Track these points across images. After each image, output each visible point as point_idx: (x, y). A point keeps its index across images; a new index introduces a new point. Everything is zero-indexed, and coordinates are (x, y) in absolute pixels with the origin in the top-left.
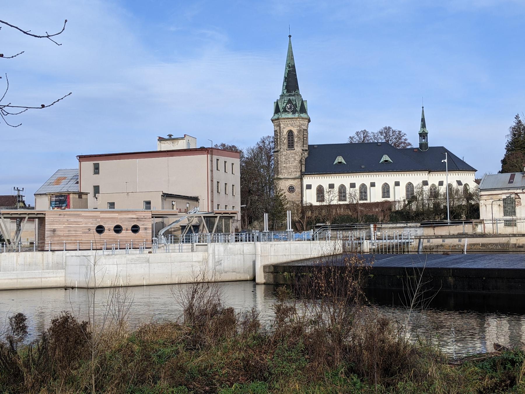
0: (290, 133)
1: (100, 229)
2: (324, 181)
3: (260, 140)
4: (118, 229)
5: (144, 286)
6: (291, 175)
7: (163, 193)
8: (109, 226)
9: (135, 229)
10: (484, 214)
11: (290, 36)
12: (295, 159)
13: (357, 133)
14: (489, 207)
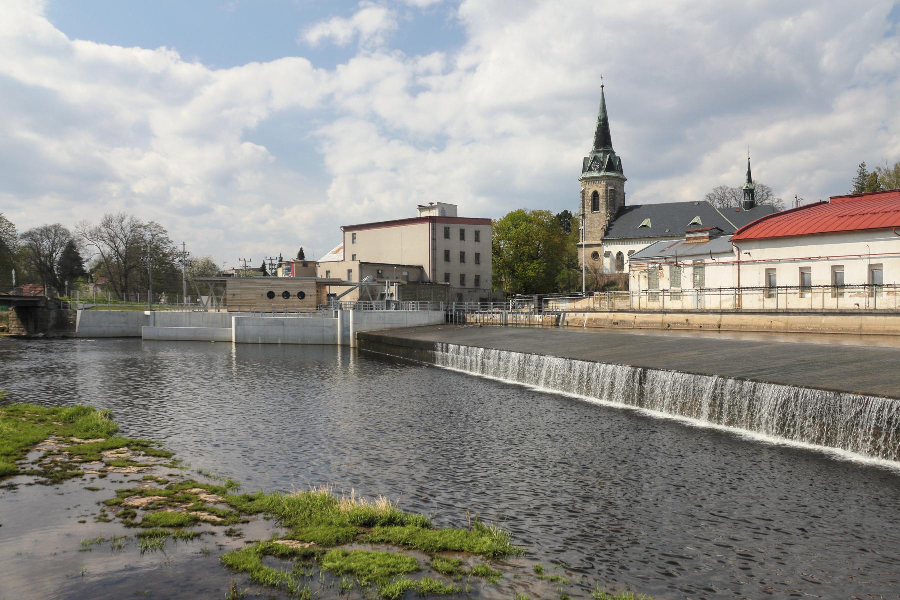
0: (596, 194)
1: (271, 295)
3: (137, 219)
4: (287, 295)
5: (308, 345)
6: (595, 241)
7: (360, 263)
8: (279, 292)
9: (302, 295)
10: (633, 286)
11: (603, 87)
12: (600, 223)
14: (637, 278)
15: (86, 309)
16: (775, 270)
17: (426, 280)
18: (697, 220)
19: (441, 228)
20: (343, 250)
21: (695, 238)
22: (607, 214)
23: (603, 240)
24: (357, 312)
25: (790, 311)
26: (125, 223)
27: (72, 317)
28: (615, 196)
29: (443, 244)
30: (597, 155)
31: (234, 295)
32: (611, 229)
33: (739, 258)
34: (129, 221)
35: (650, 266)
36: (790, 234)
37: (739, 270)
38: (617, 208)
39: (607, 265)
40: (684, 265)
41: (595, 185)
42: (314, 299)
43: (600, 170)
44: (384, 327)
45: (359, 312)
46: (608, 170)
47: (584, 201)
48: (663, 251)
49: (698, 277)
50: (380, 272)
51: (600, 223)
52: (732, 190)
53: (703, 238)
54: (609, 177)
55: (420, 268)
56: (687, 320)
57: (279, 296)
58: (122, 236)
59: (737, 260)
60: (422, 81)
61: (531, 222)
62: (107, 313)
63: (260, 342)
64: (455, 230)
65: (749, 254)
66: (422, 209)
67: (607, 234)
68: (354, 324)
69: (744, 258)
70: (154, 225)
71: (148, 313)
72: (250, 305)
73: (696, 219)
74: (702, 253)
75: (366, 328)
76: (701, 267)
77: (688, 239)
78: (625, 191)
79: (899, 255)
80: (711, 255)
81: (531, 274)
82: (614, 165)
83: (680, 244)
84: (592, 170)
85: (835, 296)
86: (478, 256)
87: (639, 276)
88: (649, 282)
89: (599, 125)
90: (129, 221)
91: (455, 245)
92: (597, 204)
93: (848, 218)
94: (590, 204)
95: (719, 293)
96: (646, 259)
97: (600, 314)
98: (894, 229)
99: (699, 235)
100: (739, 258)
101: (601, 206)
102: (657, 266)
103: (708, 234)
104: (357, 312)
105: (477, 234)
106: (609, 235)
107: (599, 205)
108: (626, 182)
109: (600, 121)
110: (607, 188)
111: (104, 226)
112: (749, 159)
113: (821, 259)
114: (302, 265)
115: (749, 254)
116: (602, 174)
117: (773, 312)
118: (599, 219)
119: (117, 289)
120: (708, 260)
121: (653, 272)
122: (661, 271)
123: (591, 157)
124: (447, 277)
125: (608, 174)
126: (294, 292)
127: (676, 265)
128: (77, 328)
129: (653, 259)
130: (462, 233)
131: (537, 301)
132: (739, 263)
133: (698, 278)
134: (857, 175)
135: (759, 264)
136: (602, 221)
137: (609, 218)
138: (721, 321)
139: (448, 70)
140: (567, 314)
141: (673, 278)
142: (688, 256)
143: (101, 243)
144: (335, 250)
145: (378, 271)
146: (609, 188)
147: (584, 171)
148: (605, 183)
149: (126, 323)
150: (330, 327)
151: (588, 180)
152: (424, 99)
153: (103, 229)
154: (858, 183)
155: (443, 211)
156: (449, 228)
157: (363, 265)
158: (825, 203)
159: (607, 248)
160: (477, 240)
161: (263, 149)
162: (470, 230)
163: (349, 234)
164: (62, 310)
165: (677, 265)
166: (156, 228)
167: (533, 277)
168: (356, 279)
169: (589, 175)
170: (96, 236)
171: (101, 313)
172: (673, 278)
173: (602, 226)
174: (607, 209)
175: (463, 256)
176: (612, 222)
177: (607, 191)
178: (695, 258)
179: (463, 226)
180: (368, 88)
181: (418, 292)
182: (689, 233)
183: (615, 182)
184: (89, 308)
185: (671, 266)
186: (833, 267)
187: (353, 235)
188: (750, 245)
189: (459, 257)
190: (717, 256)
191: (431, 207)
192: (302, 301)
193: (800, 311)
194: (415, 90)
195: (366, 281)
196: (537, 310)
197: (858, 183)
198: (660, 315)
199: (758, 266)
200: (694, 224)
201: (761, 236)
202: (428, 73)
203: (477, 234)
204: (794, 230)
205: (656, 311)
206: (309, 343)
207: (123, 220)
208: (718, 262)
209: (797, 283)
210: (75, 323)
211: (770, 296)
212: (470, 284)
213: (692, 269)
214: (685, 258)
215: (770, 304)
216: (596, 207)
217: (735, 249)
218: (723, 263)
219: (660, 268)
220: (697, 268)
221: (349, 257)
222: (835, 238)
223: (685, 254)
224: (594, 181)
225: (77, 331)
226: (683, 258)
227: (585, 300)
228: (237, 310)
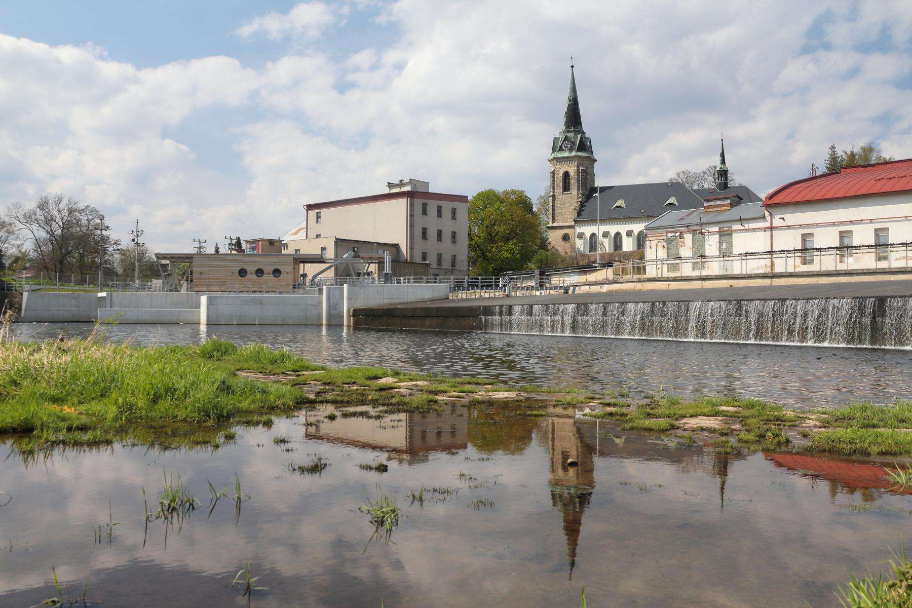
0: (566, 174)
2: (598, 229)
4: (260, 272)
6: (566, 222)
7: (336, 239)
8: (251, 269)
9: (277, 272)
11: (572, 67)
12: (571, 204)
13: (678, 175)
14: (654, 248)
15: (32, 291)
17: (402, 259)
18: (672, 200)
19: (418, 203)
20: (305, 230)
21: (715, 206)
22: (578, 195)
23: (575, 221)
24: (352, 286)
25: (853, 272)
26: (62, 205)
27: (17, 299)
29: (420, 222)
30: (568, 135)
31: (201, 273)
32: (584, 210)
33: (771, 224)
34: (67, 202)
35: (669, 235)
36: (842, 195)
37: (772, 236)
38: (588, 188)
39: (580, 244)
40: (709, 232)
41: (565, 165)
42: (291, 276)
43: (571, 150)
44: (382, 302)
45: (355, 286)
46: (579, 149)
47: (553, 181)
48: (682, 219)
49: (724, 245)
50: (356, 249)
51: (571, 204)
52: (695, 174)
53: (724, 205)
54: (580, 157)
55: (396, 247)
56: (731, 286)
57: (251, 273)
58: (58, 220)
59: (770, 225)
60: (350, 77)
61: (502, 202)
62: (56, 295)
63: (235, 323)
64: (432, 206)
65: (783, 219)
66: (392, 186)
67: (579, 215)
68: (349, 299)
69: (777, 222)
70: (90, 208)
71: (104, 294)
72: (220, 283)
73: (671, 199)
74: (730, 219)
75: (362, 304)
76: (728, 235)
77: (706, 207)
80: (741, 221)
81: (506, 255)
82: (584, 146)
83: (695, 214)
84: (563, 150)
86: (454, 235)
87: (657, 246)
88: (668, 252)
89: (569, 105)
90: (67, 202)
91: (432, 223)
92: (567, 185)
93: (886, 181)
94: (561, 184)
96: (665, 227)
97: (623, 284)
99: (718, 203)
100: (771, 224)
101: (572, 187)
102: (678, 234)
103: (729, 202)
104: (352, 286)
105: (454, 211)
106: (582, 215)
107: (569, 186)
109: (570, 101)
110: (578, 168)
111: (39, 208)
112: (722, 140)
113: (863, 222)
114: (268, 243)
115: (783, 219)
116: (574, 154)
117: (834, 273)
119: (51, 276)
121: (672, 241)
122: (682, 240)
123: (562, 137)
124: (424, 256)
125: (580, 154)
126: (268, 269)
127: (699, 232)
128: (23, 312)
129: (673, 228)
130: (440, 210)
131: (538, 277)
132: (772, 228)
133: (724, 246)
134: (827, 157)
135: (794, 228)
136: (573, 202)
137: (580, 199)
139: (375, 67)
140: (577, 288)
141: (696, 247)
142: (714, 223)
143: (35, 227)
145: (354, 248)
147: (553, 152)
148: (576, 163)
149: (76, 306)
150: (314, 305)
151: (558, 160)
152: (352, 96)
153: (38, 212)
154: (830, 164)
155: (414, 186)
156: (426, 204)
157: (339, 242)
159: (579, 230)
160: (454, 217)
161: (183, 147)
162: (447, 206)
163: (313, 213)
164: (6, 291)
165: (701, 233)
166: (92, 212)
167: (507, 258)
168: (330, 254)
169: (560, 155)
170: (29, 218)
171: (50, 294)
172: (696, 247)
173: (573, 207)
174: (578, 190)
175: (440, 234)
176: (584, 203)
177: (578, 171)
178: (721, 225)
179: (440, 203)
180: (296, 84)
181: (397, 271)
182: (707, 201)
183: (586, 162)
184: (36, 290)
185: (694, 235)
186: (876, 230)
187: (317, 213)
188: (784, 209)
190: (746, 222)
191: (401, 184)
192: (277, 279)
193: (865, 271)
194: (342, 87)
195: (346, 257)
197: (830, 164)
198: (699, 282)
199: (793, 231)
201: (797, 199)
202: (357, 69)
203: (454, 211)
205: (693, 278)
206: (290, 323)
207: (60, 200)
208: (747, 228)
210: (21, 305)
212: (447, 264)
213: (717, 237)
214: (709, 226)
216: (566, 188)
217: (767, 213)
218: (754, 229)
219: (681, 236)
220: (724, 235)
221: (312, 235)
222: (879, 200)
223: (710, 221)
224: (570, 161)
225: (22, 315)
226: (707, 226)
227: (600, 271)
228: (205, 289)
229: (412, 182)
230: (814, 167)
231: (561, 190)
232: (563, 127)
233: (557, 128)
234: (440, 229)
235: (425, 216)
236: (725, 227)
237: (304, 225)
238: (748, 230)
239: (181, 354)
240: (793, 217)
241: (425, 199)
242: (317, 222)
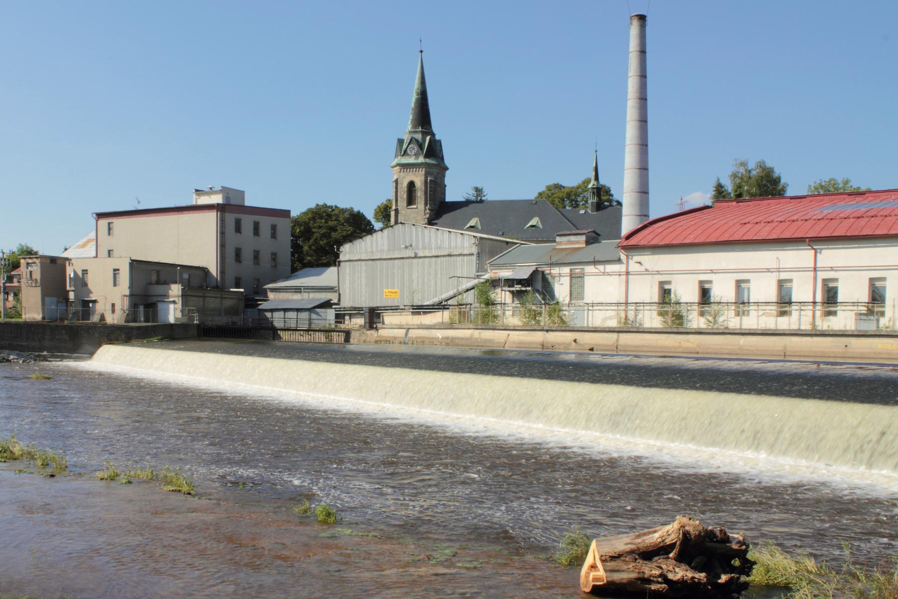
0: (411, 185)
7: (132, 260)
11: (421, 52)
16: (747, 281)
19: (230, 218)
20: (94, 243)
22: (425, 210)
28: (435, 188)
29: (233, 240)
36: (701, 241)
37: (627, 282)
47: (397, 192)
55: (204, 271)
65: (640, 263)
78: (446, 182)
79: (897, 267)
80: (595, 262)
82: (434, 151)
85: (737, 314)
94: (405, 196)
95: (616, 308)
98: (807, 240)
105: (274, 228)
108: (447, 172)
114: (49, 261)
118: (414, 215)
120: (589, 269)
123: (406, 138)
125: (428, 161)
136: (419, 218)
137: (428, 216)
138: (617, 340)
142: (565, 264)
144: (81, 243)
146: (429, 179)
148: (424, 172)
155: (226, 198)
158: (707, 207)
160: (274, 235)
163: (104, 223)
174: (426, 204)
177: (426, 181)
179: (257, 218)
183: (435, 170)
189: (252, 257)
196: (367, 325)
200: (532, 226)
203: (274, 228)
204: (692, 236)
209: (773, 297)
211: (783, 313)
215: (783, 323)
221: (103, 252)
229: (225, 191)
230: (683, 201)
231: (405, 204)
232: (409, 127)
233: (405, 127)
234: (258, 250)
235: (239, 234)
236: (578, 269)
237: (93, 235)
238: (604, 274)
239: (173, 478)
240: (650, 261)
241: (238, 213)
242: (109, 234)
